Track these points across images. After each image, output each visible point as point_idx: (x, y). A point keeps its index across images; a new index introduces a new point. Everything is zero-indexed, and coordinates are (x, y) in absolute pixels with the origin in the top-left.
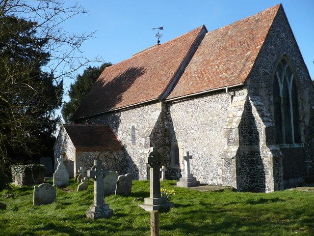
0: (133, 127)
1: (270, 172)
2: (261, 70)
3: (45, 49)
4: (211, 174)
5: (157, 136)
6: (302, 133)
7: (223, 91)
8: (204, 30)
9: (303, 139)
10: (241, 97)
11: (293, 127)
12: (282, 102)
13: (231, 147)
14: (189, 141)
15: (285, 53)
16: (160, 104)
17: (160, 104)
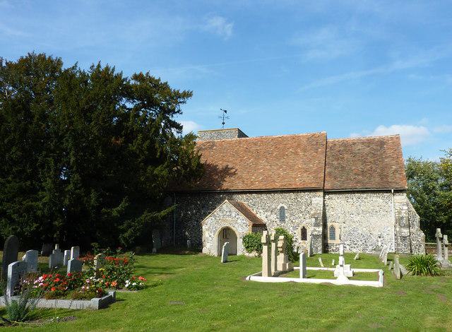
7: (390, 191)
10: (402, 198)
16: (322, 194)
17: (322, 194)
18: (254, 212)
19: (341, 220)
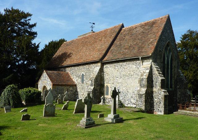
0: (83, 74)
1: (162, 103)
2: (158, 49)
3: (34, 30)
4: (127, 102)
6: (173, 83)
7: (138, 59)
8: (123, 26)
9: (173, 86)
10: (148, 63)
11: (170, 80)
12: (166, 66)
13: (142, 88)
14: (115, 83)
15: (169, 41)
16: (99, 64)
17: (99, 64)
18: (72, 78)
19: (111, 82)
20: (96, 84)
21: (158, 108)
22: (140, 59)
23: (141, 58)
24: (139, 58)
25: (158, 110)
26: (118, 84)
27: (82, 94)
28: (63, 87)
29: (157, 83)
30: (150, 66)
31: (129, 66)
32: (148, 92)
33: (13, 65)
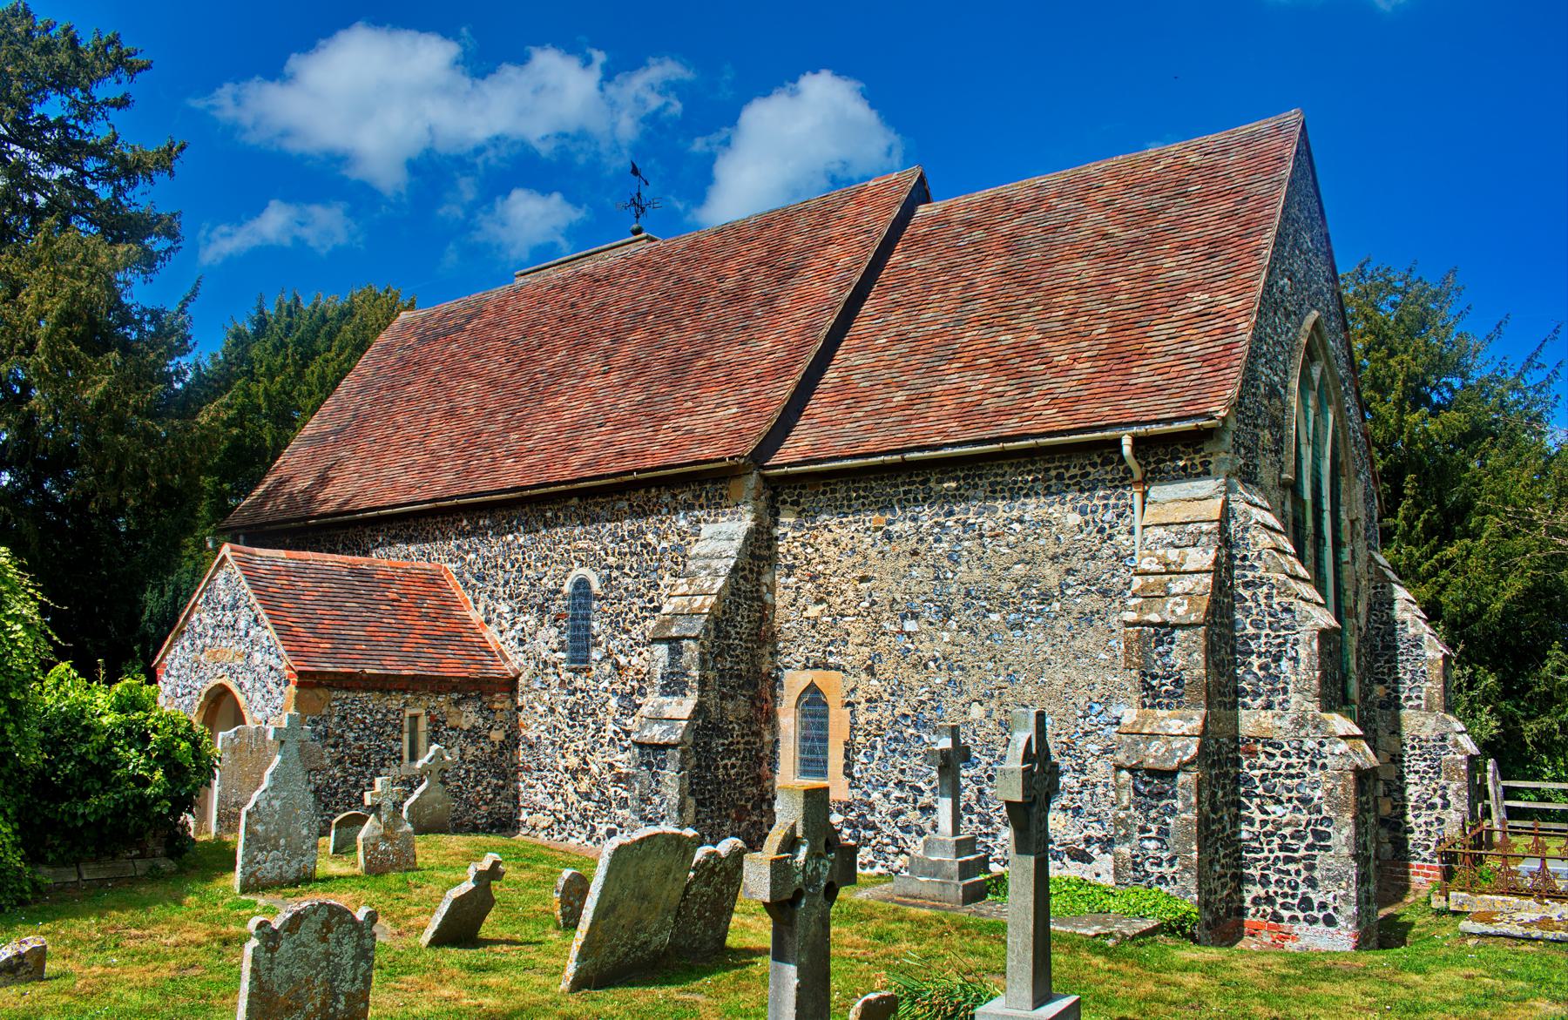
0: (582, 584)
5: (728, 636)
13: (1159, 713)
14: (887, 666)
19: (856, 654)
20: (711, 675)
21: (1302, 889)
22: (1127, 450)
23: (1137, 440)
24: (1117, 443)
25: (1306, 903)
26: (915, 679)
27: (573, 761)
28: (395, 702)
29: (1285, 664)
30: (1214, 508)
31: (1016, 514)
32: (1213, 747)
33: (117, 214)
